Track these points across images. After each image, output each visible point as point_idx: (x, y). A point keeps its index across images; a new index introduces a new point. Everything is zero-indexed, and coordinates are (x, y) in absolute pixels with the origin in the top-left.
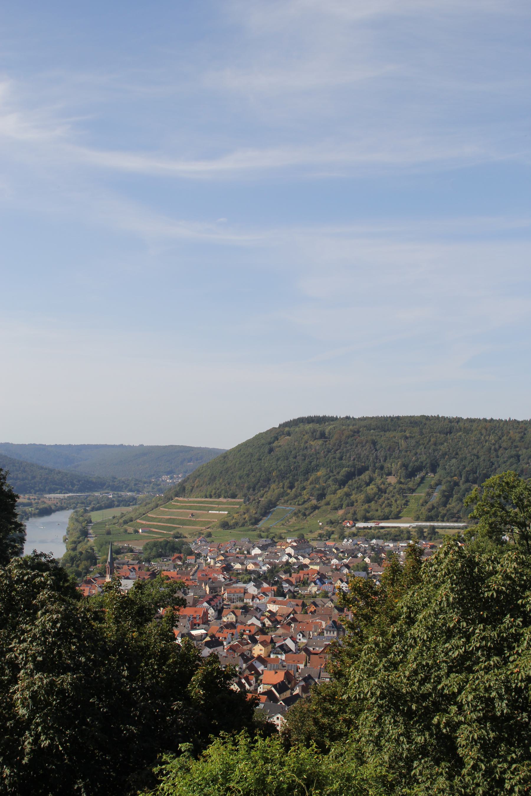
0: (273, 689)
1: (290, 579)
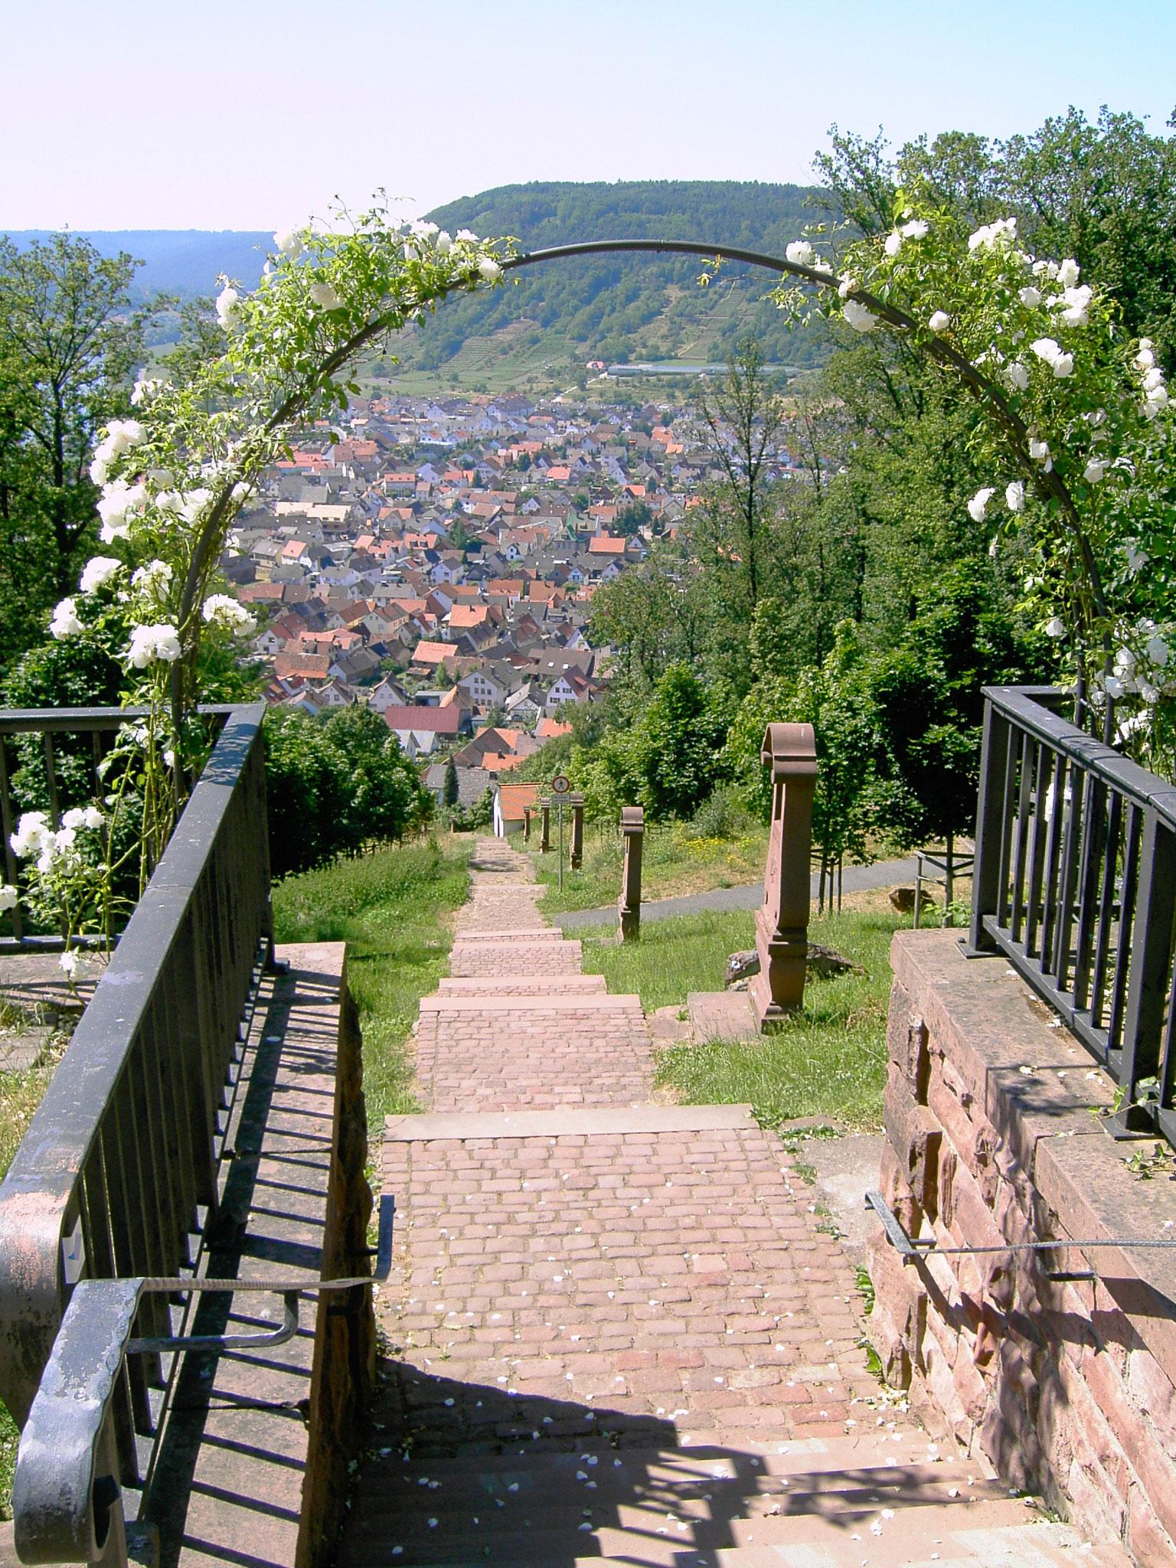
0: (466, 634)
1: (496, 458)
